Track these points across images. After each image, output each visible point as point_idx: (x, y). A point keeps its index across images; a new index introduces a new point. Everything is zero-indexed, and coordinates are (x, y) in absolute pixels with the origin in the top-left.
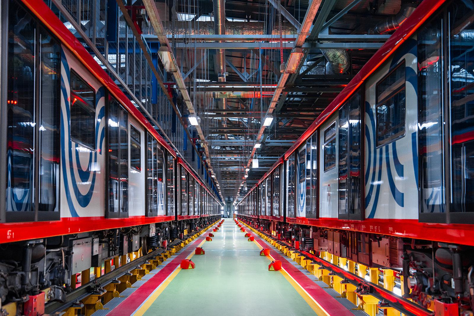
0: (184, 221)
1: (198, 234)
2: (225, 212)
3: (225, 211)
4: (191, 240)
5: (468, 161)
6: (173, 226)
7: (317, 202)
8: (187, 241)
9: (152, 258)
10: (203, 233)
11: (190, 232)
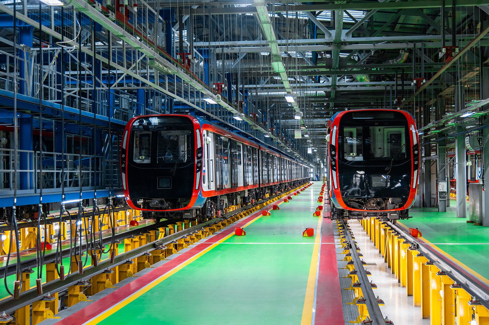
0: (265, 187)
1: (279, 197)
2: (315, 175)
3: (314, 173)
4: (272, 201)
5: (176, 207)
6: (258, 191)
7: (409, 140)
8: (268, 202)
9: (246, 210)
10: (284, 196)
11: (271, 195)
